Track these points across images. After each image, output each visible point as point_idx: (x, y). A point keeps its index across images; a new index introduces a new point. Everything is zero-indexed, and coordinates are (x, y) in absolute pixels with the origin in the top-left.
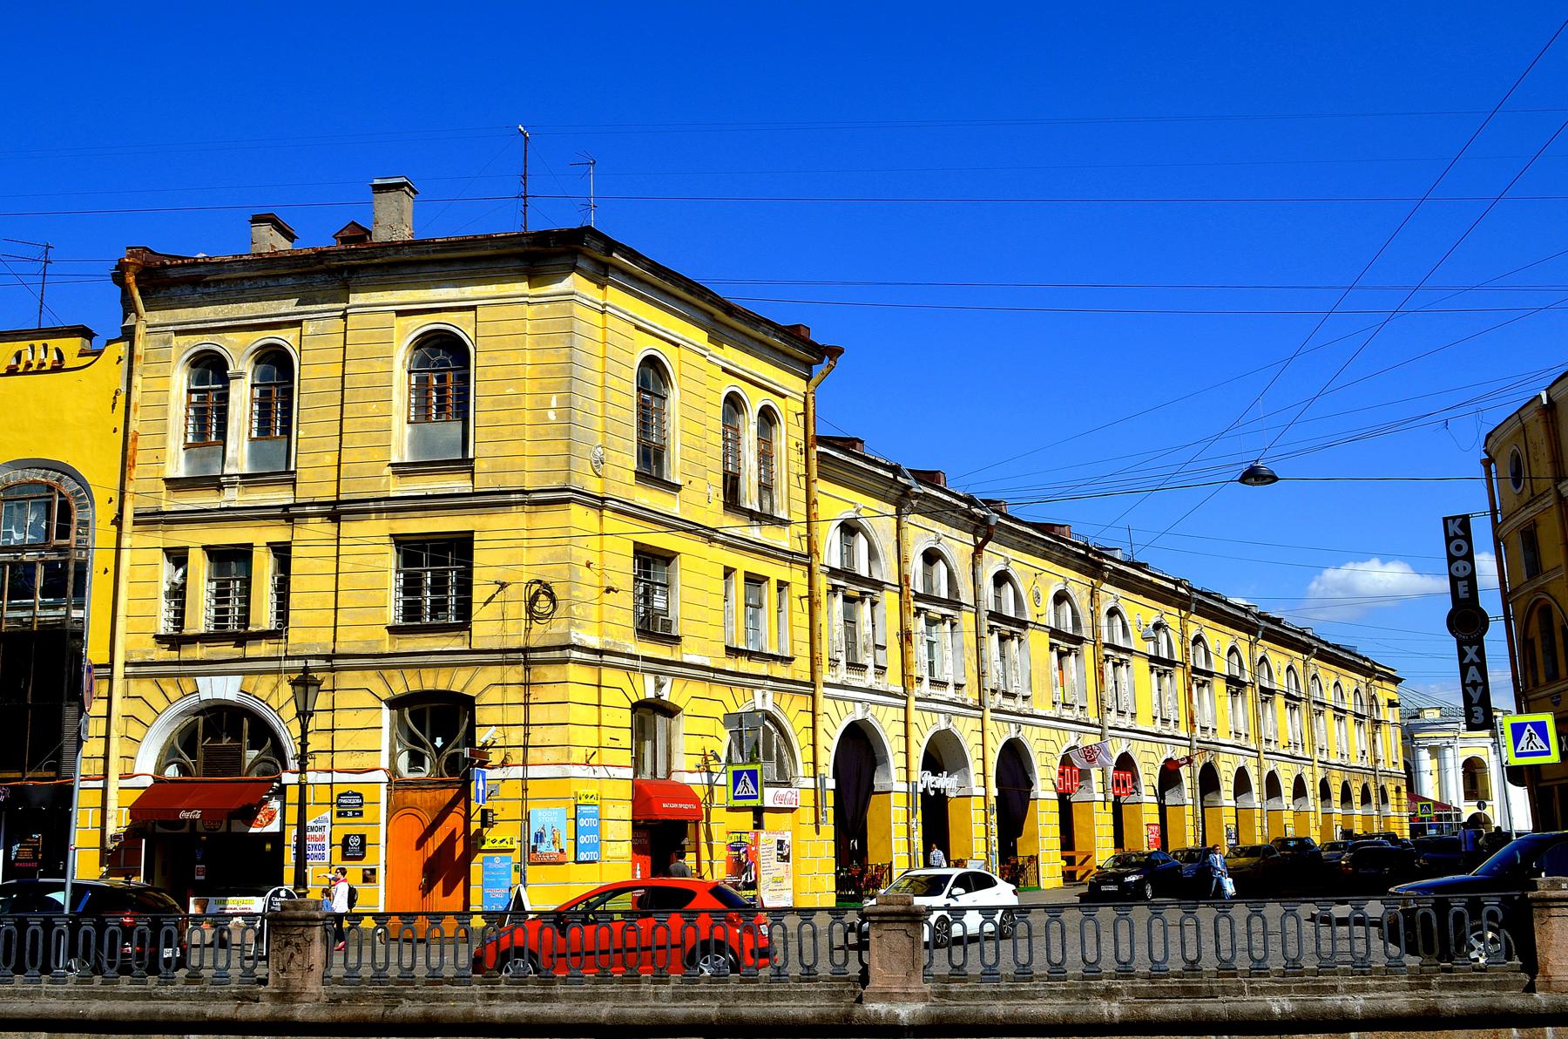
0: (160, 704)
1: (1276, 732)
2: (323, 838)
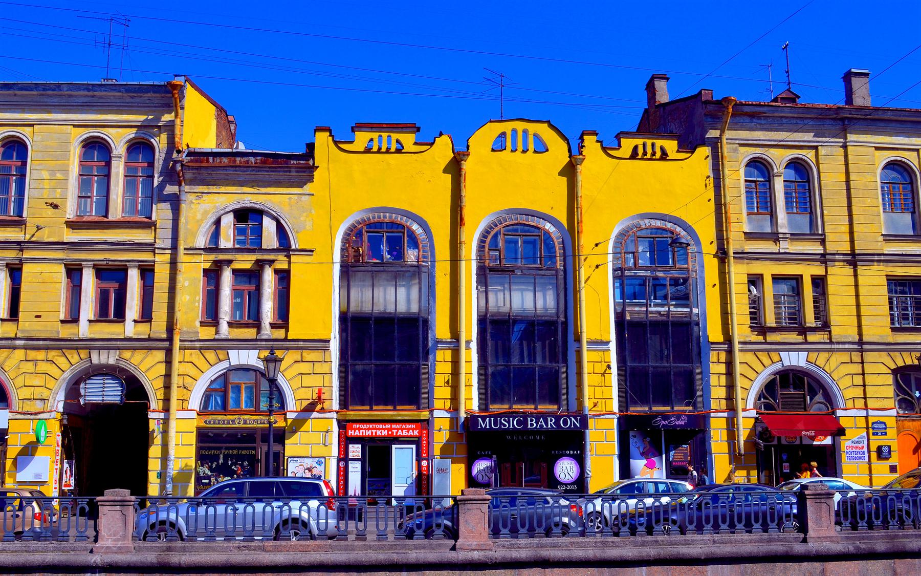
0: (759, 367)
2: (863, 448)
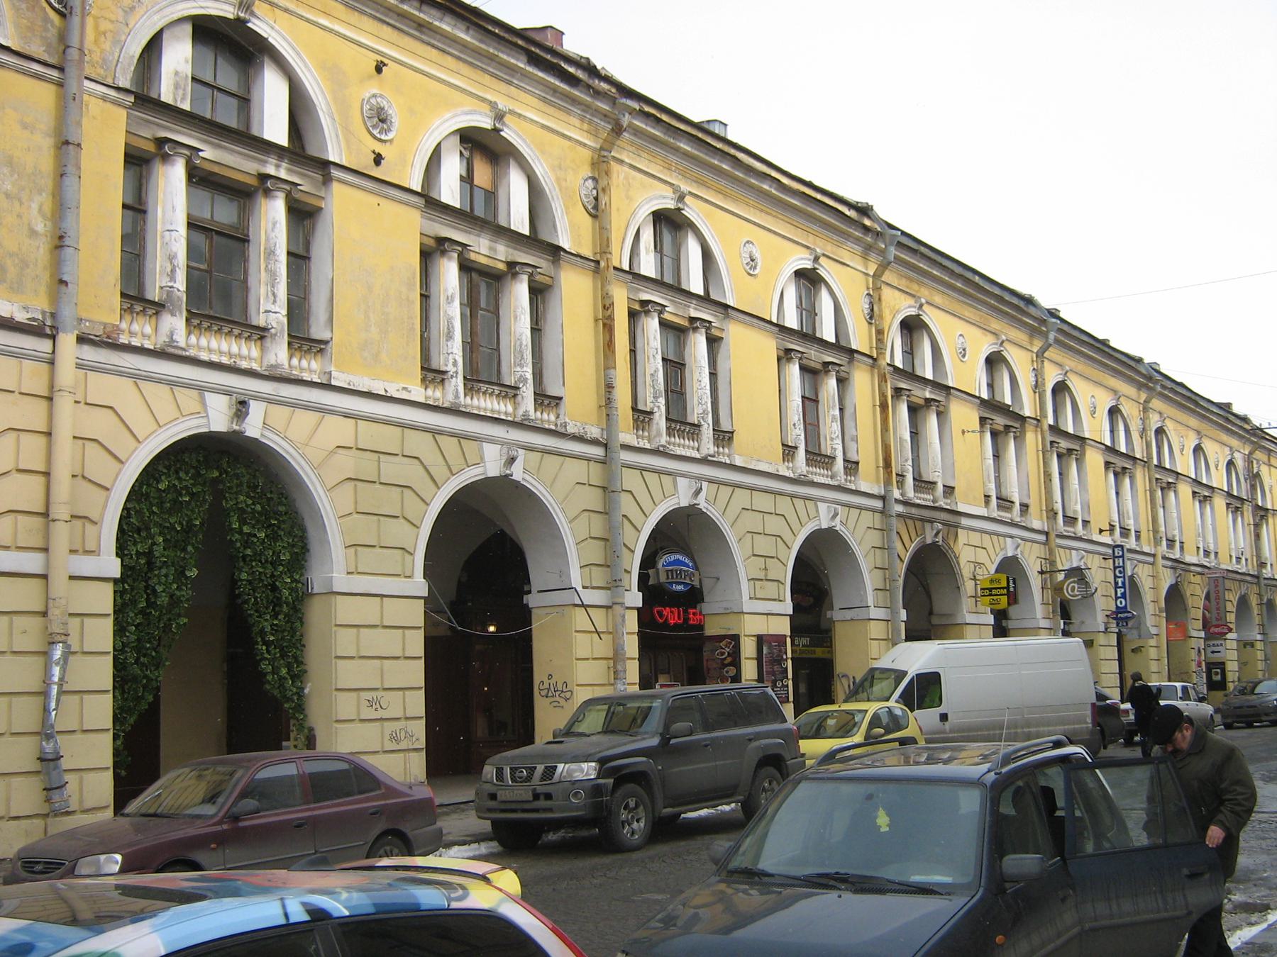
1: (1086, 507)
